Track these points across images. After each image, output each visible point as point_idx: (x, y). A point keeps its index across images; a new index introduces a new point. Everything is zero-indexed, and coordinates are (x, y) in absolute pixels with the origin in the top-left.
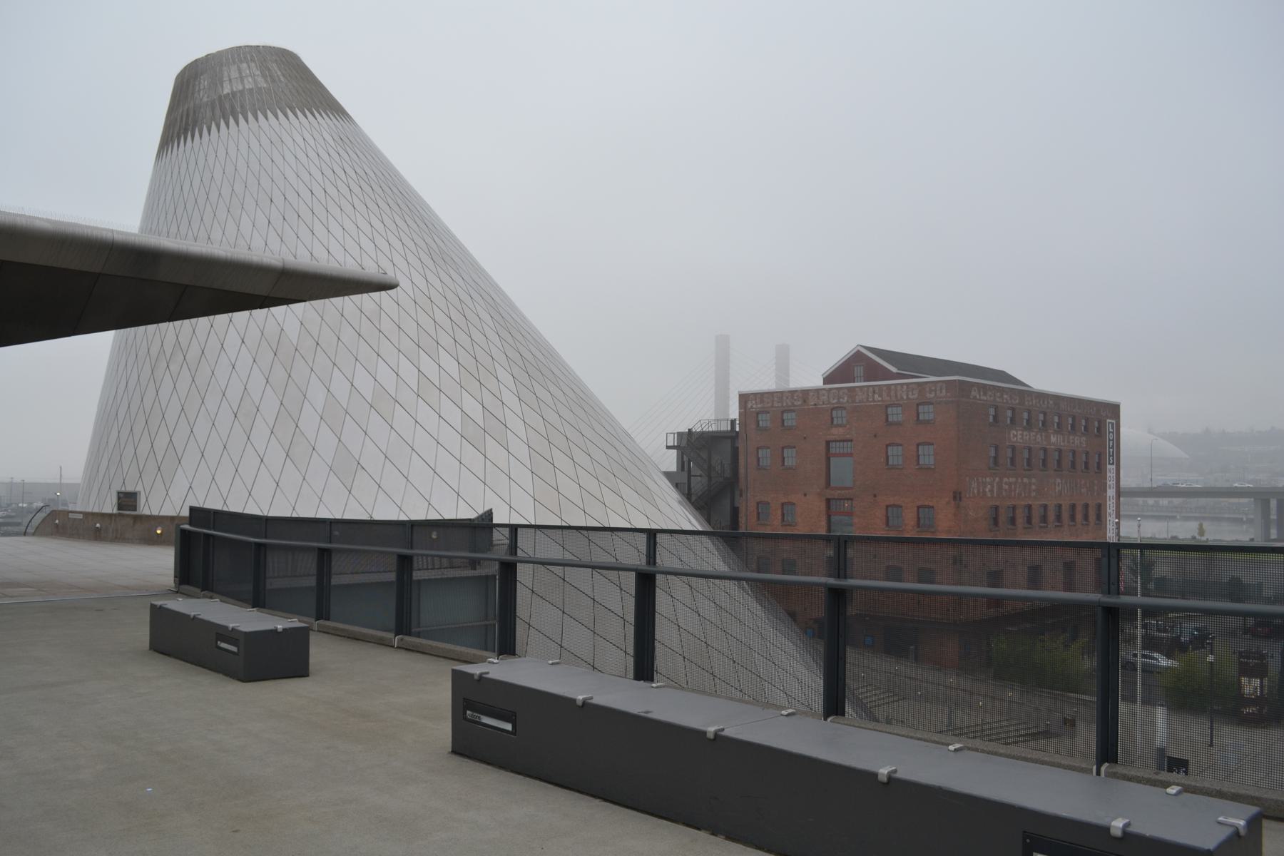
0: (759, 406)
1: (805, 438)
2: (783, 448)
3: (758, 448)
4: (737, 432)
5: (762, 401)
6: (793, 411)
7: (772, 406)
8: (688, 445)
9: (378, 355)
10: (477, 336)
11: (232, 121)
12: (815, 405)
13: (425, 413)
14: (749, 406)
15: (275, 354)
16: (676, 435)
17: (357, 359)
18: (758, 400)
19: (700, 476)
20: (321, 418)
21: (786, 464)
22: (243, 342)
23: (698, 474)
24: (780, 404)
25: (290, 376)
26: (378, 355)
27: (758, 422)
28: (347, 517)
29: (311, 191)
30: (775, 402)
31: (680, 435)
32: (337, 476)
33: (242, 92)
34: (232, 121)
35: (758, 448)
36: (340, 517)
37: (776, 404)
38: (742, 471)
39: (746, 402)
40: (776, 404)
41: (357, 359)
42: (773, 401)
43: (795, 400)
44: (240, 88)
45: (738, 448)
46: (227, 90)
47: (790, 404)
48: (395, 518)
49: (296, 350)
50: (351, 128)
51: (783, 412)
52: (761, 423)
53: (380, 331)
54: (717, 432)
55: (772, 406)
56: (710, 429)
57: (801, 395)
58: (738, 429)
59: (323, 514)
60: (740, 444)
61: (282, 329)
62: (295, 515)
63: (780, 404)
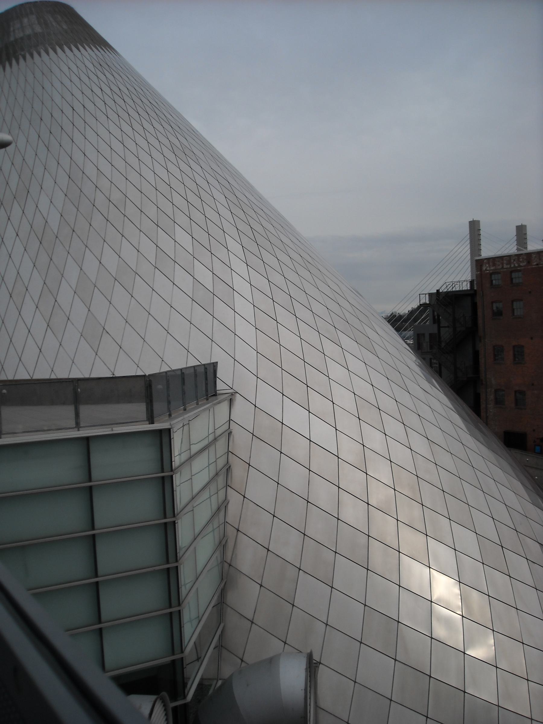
0: (492, 268)
1: (530, 292)
2: (513, 302)
3: (492, 303)
4: (476, 290)
5: (494, 265)
6: (520, 271)
7: (503, 268)
8: (437, 303)
9: (123, 236)
10: (210, 213)
11: (14, 62)
12: (537, 264)
13: (161, 283)
14: (484, 268)
15: (41, 243)
16: (427, 296)
17: (105, 241)
18: (491, 264)
19: (448, 327)
20: (75, 293)
21: (516, 314)
22: (17, 235)
23: (446, 326)
24: (508, 266)
25: (51, 260)
26: (123, 236)
27: (492, 281)
28: (94, 375)
29: (73, 108)
30: (504, 265)
31: (431, 295)
32: (86, 340)
33: (22, 38)
34: (14, 62)
35: (492, 303)
36: (66, 376)
37: (505, 266)
38: (480, 322)
39: (481, 266)
40: (505, 266)
41: (105, 241)
42: (503, 264)
43: (521, 262)
44: (21, 35)
45: (476, 303)
46: (12, 39)
47: (516, 265)
48: (133, 374)
49: (57, 237)
50: (106, 55)
51: (511, 272)
52: (494, 282)
53: (125, 216)
54: (460, 291)
55: (503, 268)
56: (454, 289)
57: (525, 257)
58: (475, 289)
59: (76, 374)
60: (478, 300)
61: (46, 222)
62: (53, 377)
63: (508, 266)
